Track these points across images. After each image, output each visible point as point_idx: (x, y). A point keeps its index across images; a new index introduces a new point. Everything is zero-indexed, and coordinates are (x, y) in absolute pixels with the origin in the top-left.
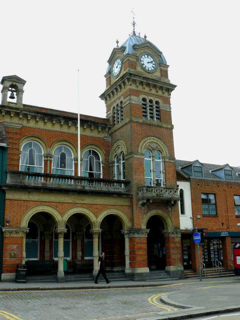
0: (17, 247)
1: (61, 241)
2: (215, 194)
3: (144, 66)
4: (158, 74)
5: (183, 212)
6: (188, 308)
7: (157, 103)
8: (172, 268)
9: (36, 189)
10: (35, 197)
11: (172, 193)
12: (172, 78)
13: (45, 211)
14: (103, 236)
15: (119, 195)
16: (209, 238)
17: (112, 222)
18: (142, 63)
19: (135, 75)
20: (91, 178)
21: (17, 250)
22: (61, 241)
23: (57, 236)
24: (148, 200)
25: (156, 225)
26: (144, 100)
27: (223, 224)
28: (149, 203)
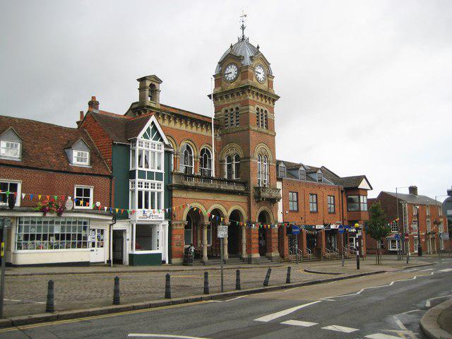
1: (205, 232)
2: (297, 193)
4: (266, 84)
6: (384, 272)
7: (266, 111)
8: (273, 254)
9: (194, 189)
10: (191, 195)
12: (277, 90)
15: (242, 193)
16: (290, 229)
17: (236, 215)
19: (255, 88)
20: (220, 180)
22: (205, 232)
23: (202, 226)
25: (263, 217)
28: (259, 199)
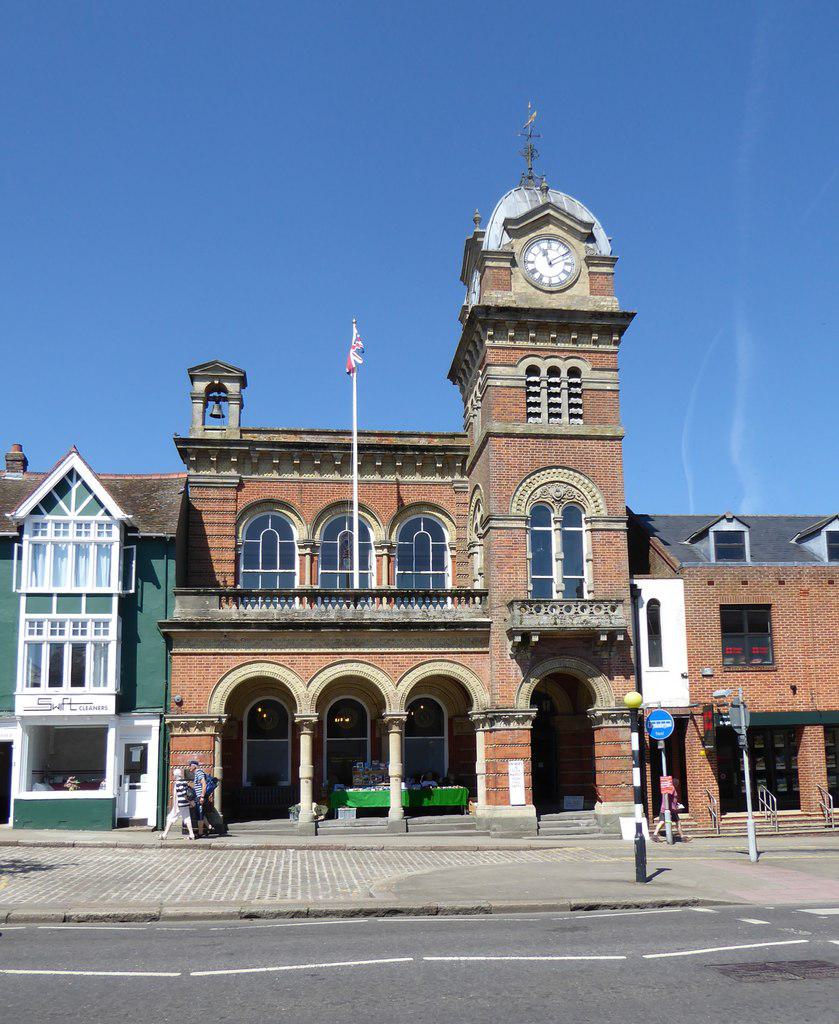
0: (199, 757)
3: (536, 276)
5: (656, 659)
7: (574, 372)
11: (602, 612)
13: (264, 674)
14: (409, 728)
18: (530, 267)
21: (813, 759)
23: (297, 729)
24: (526, 636)
26: (533, 370)
27: (794, 689)
